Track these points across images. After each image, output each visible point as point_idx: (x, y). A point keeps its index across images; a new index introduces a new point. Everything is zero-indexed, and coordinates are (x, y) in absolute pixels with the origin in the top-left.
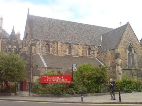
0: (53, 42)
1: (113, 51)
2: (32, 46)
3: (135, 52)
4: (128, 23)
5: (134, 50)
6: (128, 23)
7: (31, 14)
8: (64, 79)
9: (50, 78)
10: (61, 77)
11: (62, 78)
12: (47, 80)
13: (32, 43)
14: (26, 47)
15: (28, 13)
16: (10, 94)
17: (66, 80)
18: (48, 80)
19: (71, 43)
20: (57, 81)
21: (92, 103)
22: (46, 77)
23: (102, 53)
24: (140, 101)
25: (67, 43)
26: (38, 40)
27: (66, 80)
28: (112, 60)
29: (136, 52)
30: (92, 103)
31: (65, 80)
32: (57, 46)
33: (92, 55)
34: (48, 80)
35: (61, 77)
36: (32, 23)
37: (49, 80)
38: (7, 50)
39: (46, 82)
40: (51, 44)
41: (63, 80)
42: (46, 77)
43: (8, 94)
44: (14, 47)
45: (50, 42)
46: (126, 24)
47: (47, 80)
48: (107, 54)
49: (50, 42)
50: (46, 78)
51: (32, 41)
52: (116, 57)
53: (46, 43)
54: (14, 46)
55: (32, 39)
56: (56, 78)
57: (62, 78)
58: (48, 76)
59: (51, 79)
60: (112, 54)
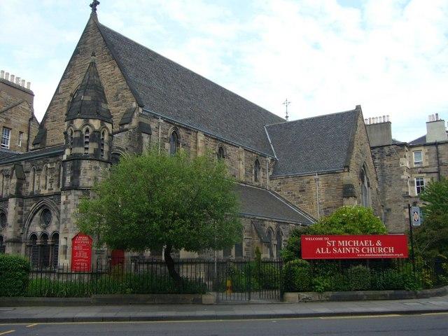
0: (187, 129)
1: (331, 177)
2: (143, 135)
3: (369, 186)
4: (358, 108)
5: (367, 178)
6: (358, 108)
7: (104, 19)
8: (383, 246)
9: (337, 244)
10: (374, 242)
11: (379, 243)
12: (325, 250)
13: (140, 123)
14: (122, 135)
15: (94, 15)
16: (196, 296)
17: (391, 249)
18: (331, 248)
19: (226, 139)
20: (361, 253)
21: (130, 319)
22: (321, 239)
23: (290, 180)
24: (446, 308)
25: (216, 139)
26: (155, 117)
27: (391, 249)
28: (327, 200)
29: (371, 184)
30: (130, 319)
31: (387, 250)
32: (196, 143)
33: (262, 181)
34: (331, 248)
35: (374, 242)
36: (100, 45)
37: (332, 251)
38: (82, 135)
39: (321, 255)
40: (182, 133)
41: (380, 250)
42: (321, 239)
43: (191, 297)
44: (107, 128)
45: (180, 127)
46: (297, 111)
47: (325, 250)
48: (308, 183)
49: (180, 127)
50: (323, 244)
51: (140, 115)
52: (344, 193)
53: (171, 131)
54: (91, 121)
55: (141, 110)
56: (356, 243)
57: (379, 243)
58: (12, 242)
59: (341, 247)
60: (328, 185)
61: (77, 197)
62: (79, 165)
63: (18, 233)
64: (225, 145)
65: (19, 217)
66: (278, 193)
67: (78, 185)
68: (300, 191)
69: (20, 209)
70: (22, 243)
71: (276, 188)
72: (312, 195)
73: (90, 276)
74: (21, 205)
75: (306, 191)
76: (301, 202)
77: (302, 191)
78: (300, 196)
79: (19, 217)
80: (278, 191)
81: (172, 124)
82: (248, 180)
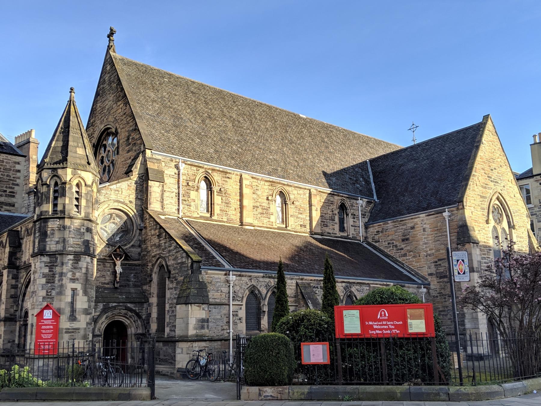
28: (438, 250)
45: (144, 179)
52: (458, 239)
61: (43, 265)
62: (46, 226)
63: (12, 311)
64: (287, 188)
65: (13, 291)
66: (377, 244)
67: (45, 249)
68: (403, 240)
69: (13, 282)
70: (16, 322)
71: (373, 239)
72: (419, 245)
73: (159, 368)
74: (16, 277)
75: (411, 239)
76: (405, 255)
77: (405, 240)
78: (403, 246)
79: (13, 291)
80: (376, 242)
81: (200, 167)
82: (327, 230)
